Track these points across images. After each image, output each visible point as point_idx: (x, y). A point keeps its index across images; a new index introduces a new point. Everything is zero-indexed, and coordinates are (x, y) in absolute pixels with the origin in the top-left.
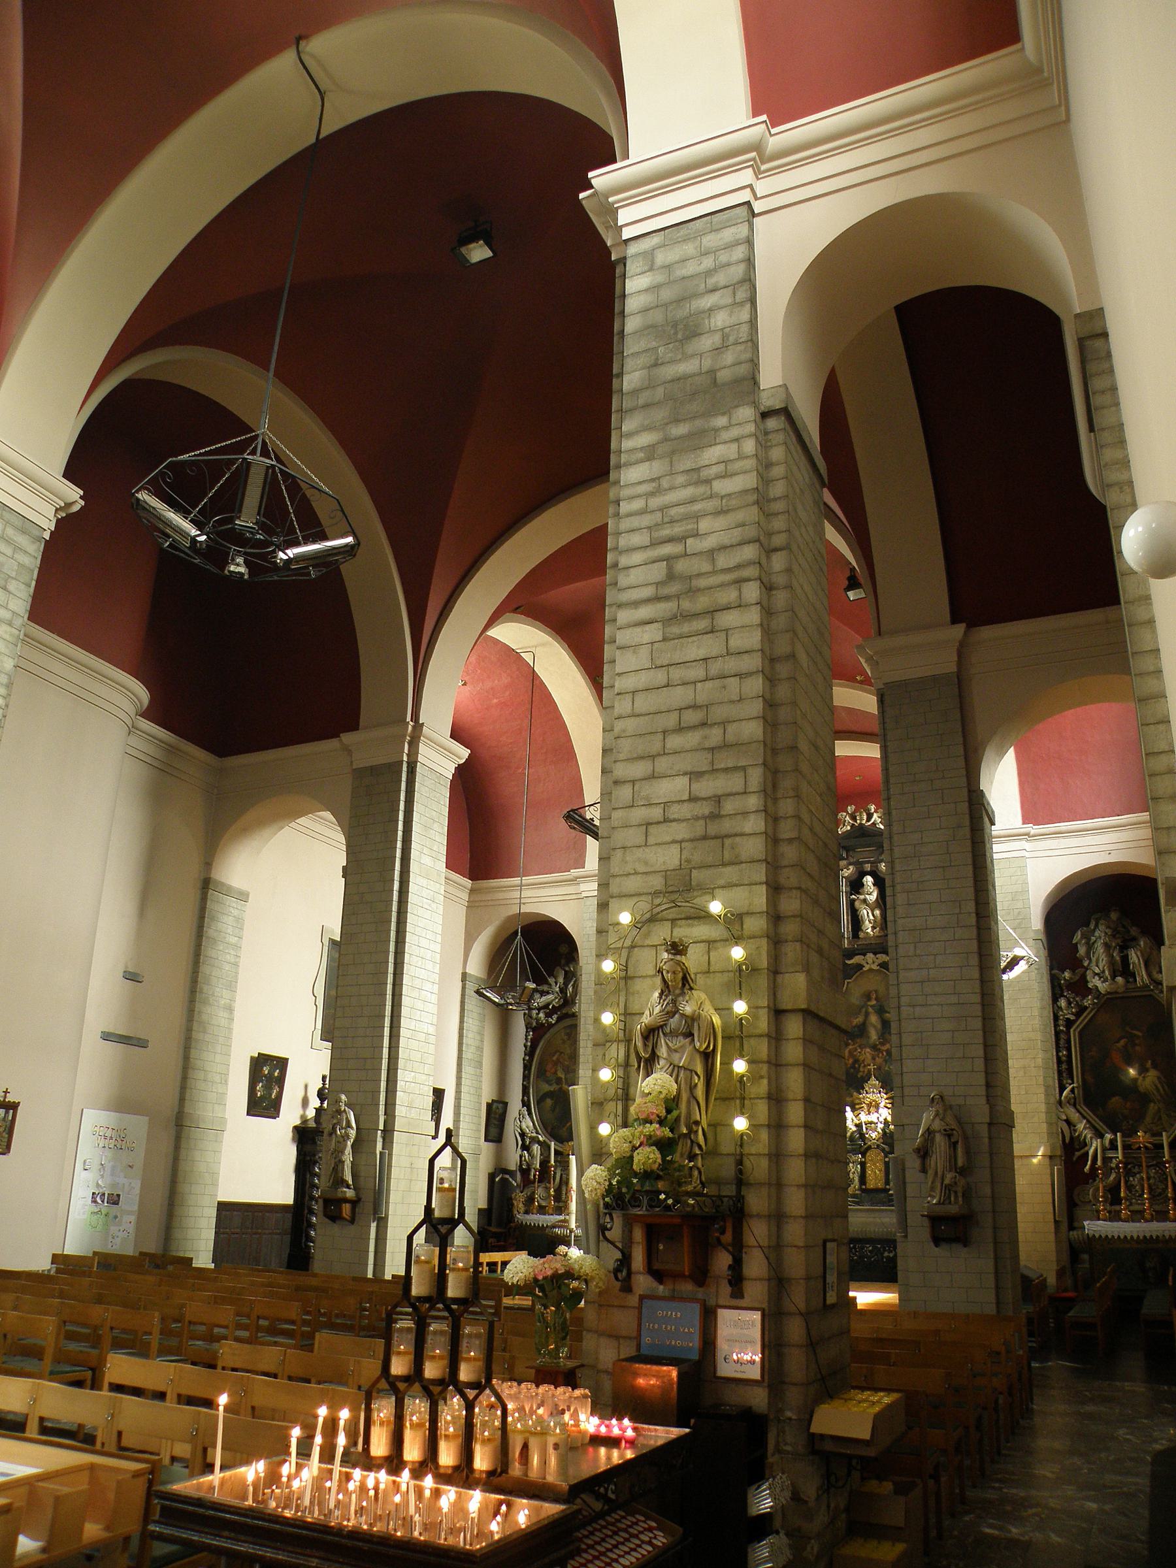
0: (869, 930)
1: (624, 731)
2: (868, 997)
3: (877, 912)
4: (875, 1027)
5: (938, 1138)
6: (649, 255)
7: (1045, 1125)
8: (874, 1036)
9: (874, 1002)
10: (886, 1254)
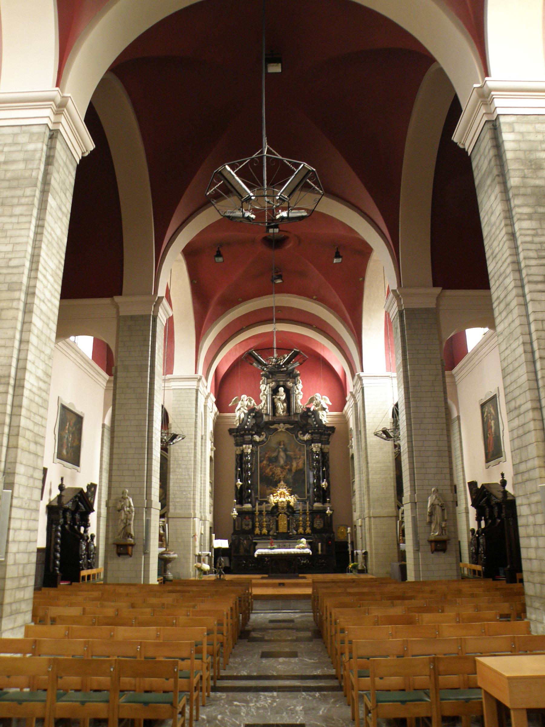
0: (281, 413)
1: (541, 336)
2: (279, 444)
3: (285, 405)
4: (283, 458)
5: (437, 507)
6: (511, 124)
7: (394, 503)
8: (282, 462)
9: (282, 446)
10: (302, 562)
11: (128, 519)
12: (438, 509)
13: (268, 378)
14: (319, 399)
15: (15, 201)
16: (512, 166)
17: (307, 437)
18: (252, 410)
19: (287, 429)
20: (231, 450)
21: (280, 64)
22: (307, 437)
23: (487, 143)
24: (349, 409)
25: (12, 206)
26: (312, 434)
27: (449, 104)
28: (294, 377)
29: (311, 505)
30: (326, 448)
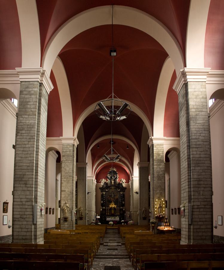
6: (156, 146)
8: (113, 196)
11: (82, 212)
12: (145, 211)
13: (110, 174)
14: (123, 180)
15: (69, 160)
16: (155, 155)
17: (119, 190)
18: (105, 183)
19: (114, 188)
20: (100, 193)
21: (116, 53)
22: (119, 190)
23: (152, 147)
24: (130, 182)
25: (68, 161)
26: (120, 189)
27: (173, 71)
28: (117, 174)
29: (120, 208)
30: (124, 193)
